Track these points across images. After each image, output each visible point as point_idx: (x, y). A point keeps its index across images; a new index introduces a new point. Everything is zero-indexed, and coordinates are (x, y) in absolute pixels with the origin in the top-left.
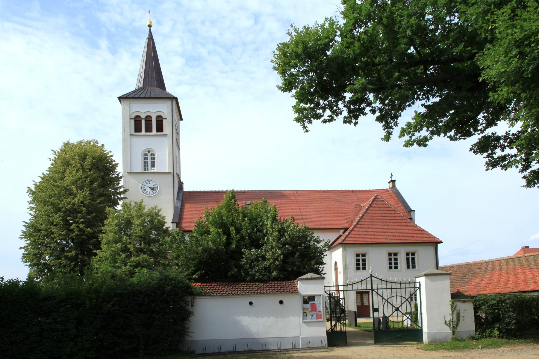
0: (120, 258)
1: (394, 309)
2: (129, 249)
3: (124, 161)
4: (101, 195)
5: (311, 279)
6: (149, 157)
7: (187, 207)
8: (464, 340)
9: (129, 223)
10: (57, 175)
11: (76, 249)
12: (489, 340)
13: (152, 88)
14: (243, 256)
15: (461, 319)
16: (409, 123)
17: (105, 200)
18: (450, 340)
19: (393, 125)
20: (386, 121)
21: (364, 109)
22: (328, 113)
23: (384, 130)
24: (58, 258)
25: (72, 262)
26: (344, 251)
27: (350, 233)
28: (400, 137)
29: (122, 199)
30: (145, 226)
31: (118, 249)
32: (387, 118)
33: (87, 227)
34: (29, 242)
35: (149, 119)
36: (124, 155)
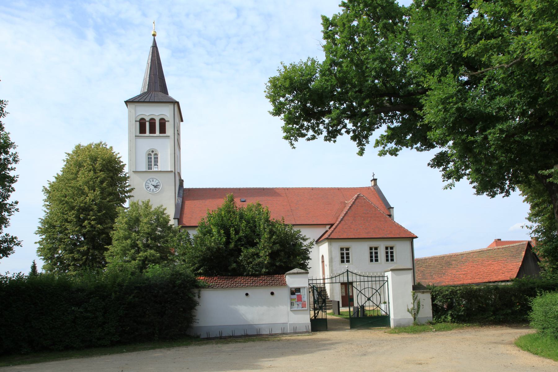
0: (130, 253)
1: (366, 299)
2: (137, 245)
3: (130, 160)
4: (110, 194)
5: (298, 273)
6: (153, 157)
7: (188, 203)
8: (423, 325)
9: (137, 221)
10: (71, 176)
11: (87, 244)
12: (443, 324)
13: (156, 93)
14: (242, 254)
15: (421, 307)
16: (382, 135)
17: (114, 199)
18: (411, 325)
19: (365, 142)
20: (359, 140)
21: (340, 130)
22: (311, 133)
23: (358, 146)
24: (71, 252)
25: (83, 256)
26: (330, 245)
27: (335, 228)
28: (375, 147)
29: (129, 197)
30: (152, 224)
31: (127, 245)
32: (360, 138)
33: (98, 224)
34: (44, 237)
35: (152, 121)
36: (130, 154)
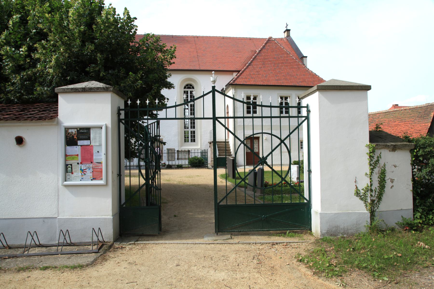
15: (388, 184)
18: (364, 230)
